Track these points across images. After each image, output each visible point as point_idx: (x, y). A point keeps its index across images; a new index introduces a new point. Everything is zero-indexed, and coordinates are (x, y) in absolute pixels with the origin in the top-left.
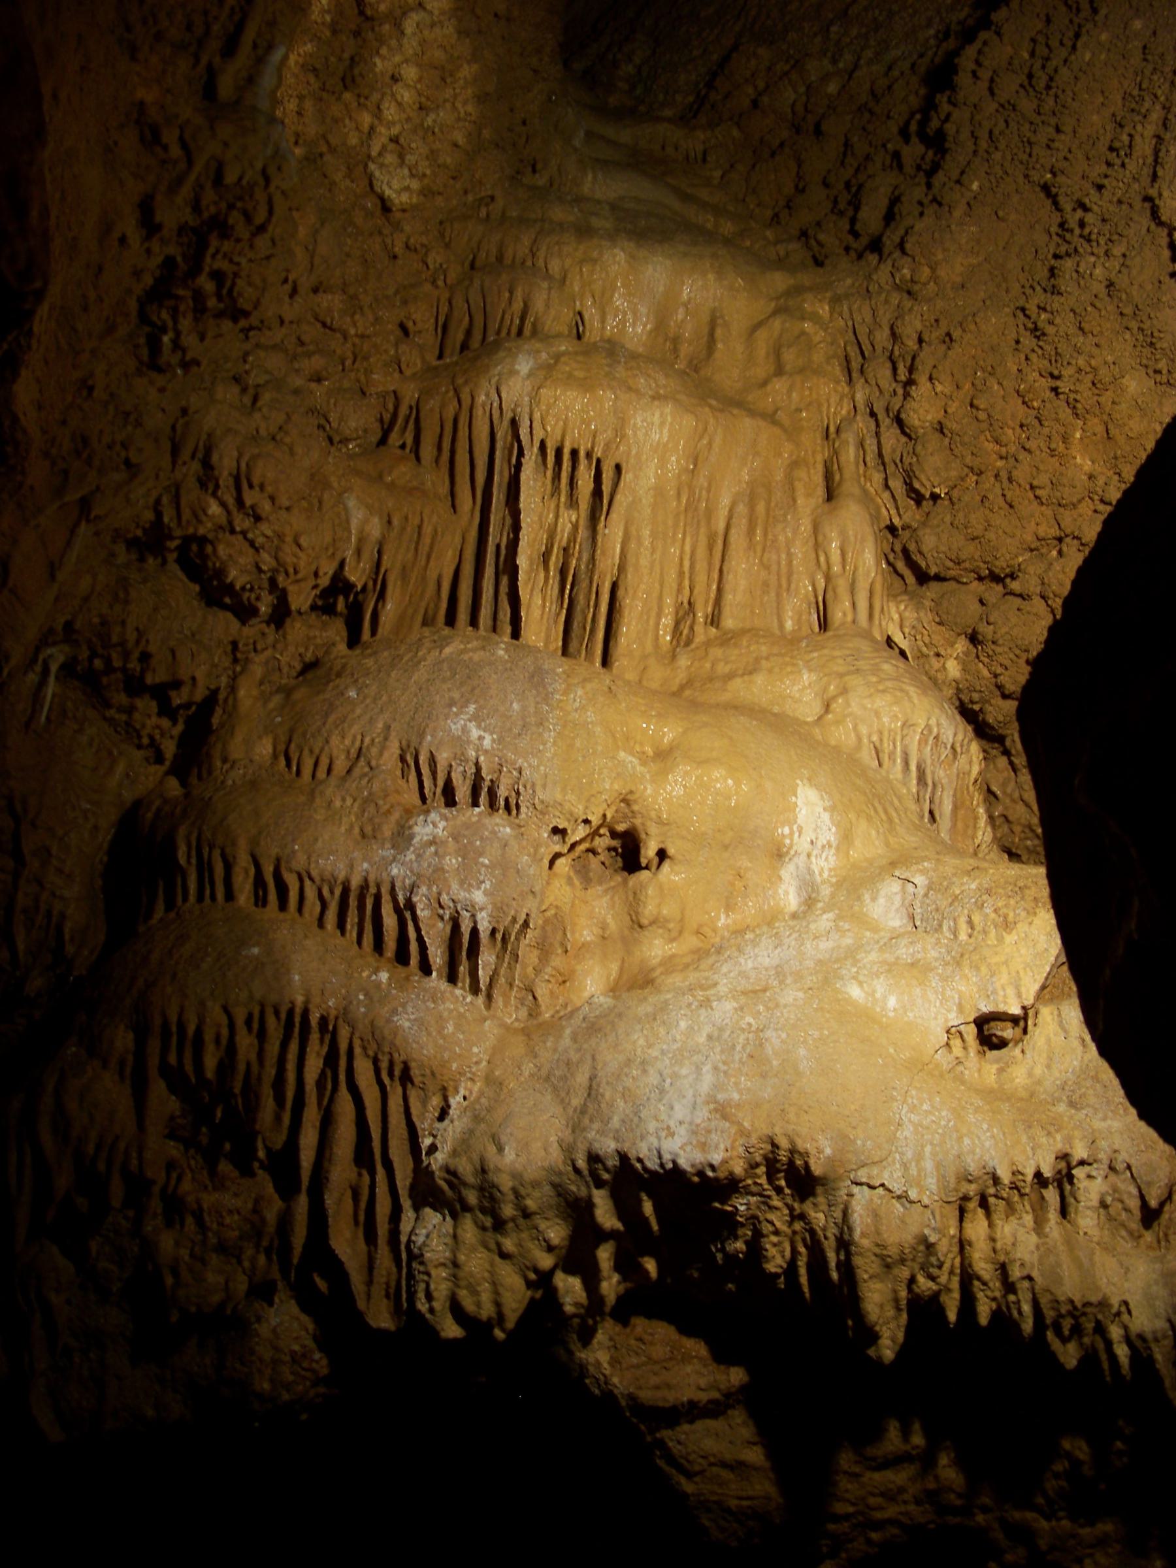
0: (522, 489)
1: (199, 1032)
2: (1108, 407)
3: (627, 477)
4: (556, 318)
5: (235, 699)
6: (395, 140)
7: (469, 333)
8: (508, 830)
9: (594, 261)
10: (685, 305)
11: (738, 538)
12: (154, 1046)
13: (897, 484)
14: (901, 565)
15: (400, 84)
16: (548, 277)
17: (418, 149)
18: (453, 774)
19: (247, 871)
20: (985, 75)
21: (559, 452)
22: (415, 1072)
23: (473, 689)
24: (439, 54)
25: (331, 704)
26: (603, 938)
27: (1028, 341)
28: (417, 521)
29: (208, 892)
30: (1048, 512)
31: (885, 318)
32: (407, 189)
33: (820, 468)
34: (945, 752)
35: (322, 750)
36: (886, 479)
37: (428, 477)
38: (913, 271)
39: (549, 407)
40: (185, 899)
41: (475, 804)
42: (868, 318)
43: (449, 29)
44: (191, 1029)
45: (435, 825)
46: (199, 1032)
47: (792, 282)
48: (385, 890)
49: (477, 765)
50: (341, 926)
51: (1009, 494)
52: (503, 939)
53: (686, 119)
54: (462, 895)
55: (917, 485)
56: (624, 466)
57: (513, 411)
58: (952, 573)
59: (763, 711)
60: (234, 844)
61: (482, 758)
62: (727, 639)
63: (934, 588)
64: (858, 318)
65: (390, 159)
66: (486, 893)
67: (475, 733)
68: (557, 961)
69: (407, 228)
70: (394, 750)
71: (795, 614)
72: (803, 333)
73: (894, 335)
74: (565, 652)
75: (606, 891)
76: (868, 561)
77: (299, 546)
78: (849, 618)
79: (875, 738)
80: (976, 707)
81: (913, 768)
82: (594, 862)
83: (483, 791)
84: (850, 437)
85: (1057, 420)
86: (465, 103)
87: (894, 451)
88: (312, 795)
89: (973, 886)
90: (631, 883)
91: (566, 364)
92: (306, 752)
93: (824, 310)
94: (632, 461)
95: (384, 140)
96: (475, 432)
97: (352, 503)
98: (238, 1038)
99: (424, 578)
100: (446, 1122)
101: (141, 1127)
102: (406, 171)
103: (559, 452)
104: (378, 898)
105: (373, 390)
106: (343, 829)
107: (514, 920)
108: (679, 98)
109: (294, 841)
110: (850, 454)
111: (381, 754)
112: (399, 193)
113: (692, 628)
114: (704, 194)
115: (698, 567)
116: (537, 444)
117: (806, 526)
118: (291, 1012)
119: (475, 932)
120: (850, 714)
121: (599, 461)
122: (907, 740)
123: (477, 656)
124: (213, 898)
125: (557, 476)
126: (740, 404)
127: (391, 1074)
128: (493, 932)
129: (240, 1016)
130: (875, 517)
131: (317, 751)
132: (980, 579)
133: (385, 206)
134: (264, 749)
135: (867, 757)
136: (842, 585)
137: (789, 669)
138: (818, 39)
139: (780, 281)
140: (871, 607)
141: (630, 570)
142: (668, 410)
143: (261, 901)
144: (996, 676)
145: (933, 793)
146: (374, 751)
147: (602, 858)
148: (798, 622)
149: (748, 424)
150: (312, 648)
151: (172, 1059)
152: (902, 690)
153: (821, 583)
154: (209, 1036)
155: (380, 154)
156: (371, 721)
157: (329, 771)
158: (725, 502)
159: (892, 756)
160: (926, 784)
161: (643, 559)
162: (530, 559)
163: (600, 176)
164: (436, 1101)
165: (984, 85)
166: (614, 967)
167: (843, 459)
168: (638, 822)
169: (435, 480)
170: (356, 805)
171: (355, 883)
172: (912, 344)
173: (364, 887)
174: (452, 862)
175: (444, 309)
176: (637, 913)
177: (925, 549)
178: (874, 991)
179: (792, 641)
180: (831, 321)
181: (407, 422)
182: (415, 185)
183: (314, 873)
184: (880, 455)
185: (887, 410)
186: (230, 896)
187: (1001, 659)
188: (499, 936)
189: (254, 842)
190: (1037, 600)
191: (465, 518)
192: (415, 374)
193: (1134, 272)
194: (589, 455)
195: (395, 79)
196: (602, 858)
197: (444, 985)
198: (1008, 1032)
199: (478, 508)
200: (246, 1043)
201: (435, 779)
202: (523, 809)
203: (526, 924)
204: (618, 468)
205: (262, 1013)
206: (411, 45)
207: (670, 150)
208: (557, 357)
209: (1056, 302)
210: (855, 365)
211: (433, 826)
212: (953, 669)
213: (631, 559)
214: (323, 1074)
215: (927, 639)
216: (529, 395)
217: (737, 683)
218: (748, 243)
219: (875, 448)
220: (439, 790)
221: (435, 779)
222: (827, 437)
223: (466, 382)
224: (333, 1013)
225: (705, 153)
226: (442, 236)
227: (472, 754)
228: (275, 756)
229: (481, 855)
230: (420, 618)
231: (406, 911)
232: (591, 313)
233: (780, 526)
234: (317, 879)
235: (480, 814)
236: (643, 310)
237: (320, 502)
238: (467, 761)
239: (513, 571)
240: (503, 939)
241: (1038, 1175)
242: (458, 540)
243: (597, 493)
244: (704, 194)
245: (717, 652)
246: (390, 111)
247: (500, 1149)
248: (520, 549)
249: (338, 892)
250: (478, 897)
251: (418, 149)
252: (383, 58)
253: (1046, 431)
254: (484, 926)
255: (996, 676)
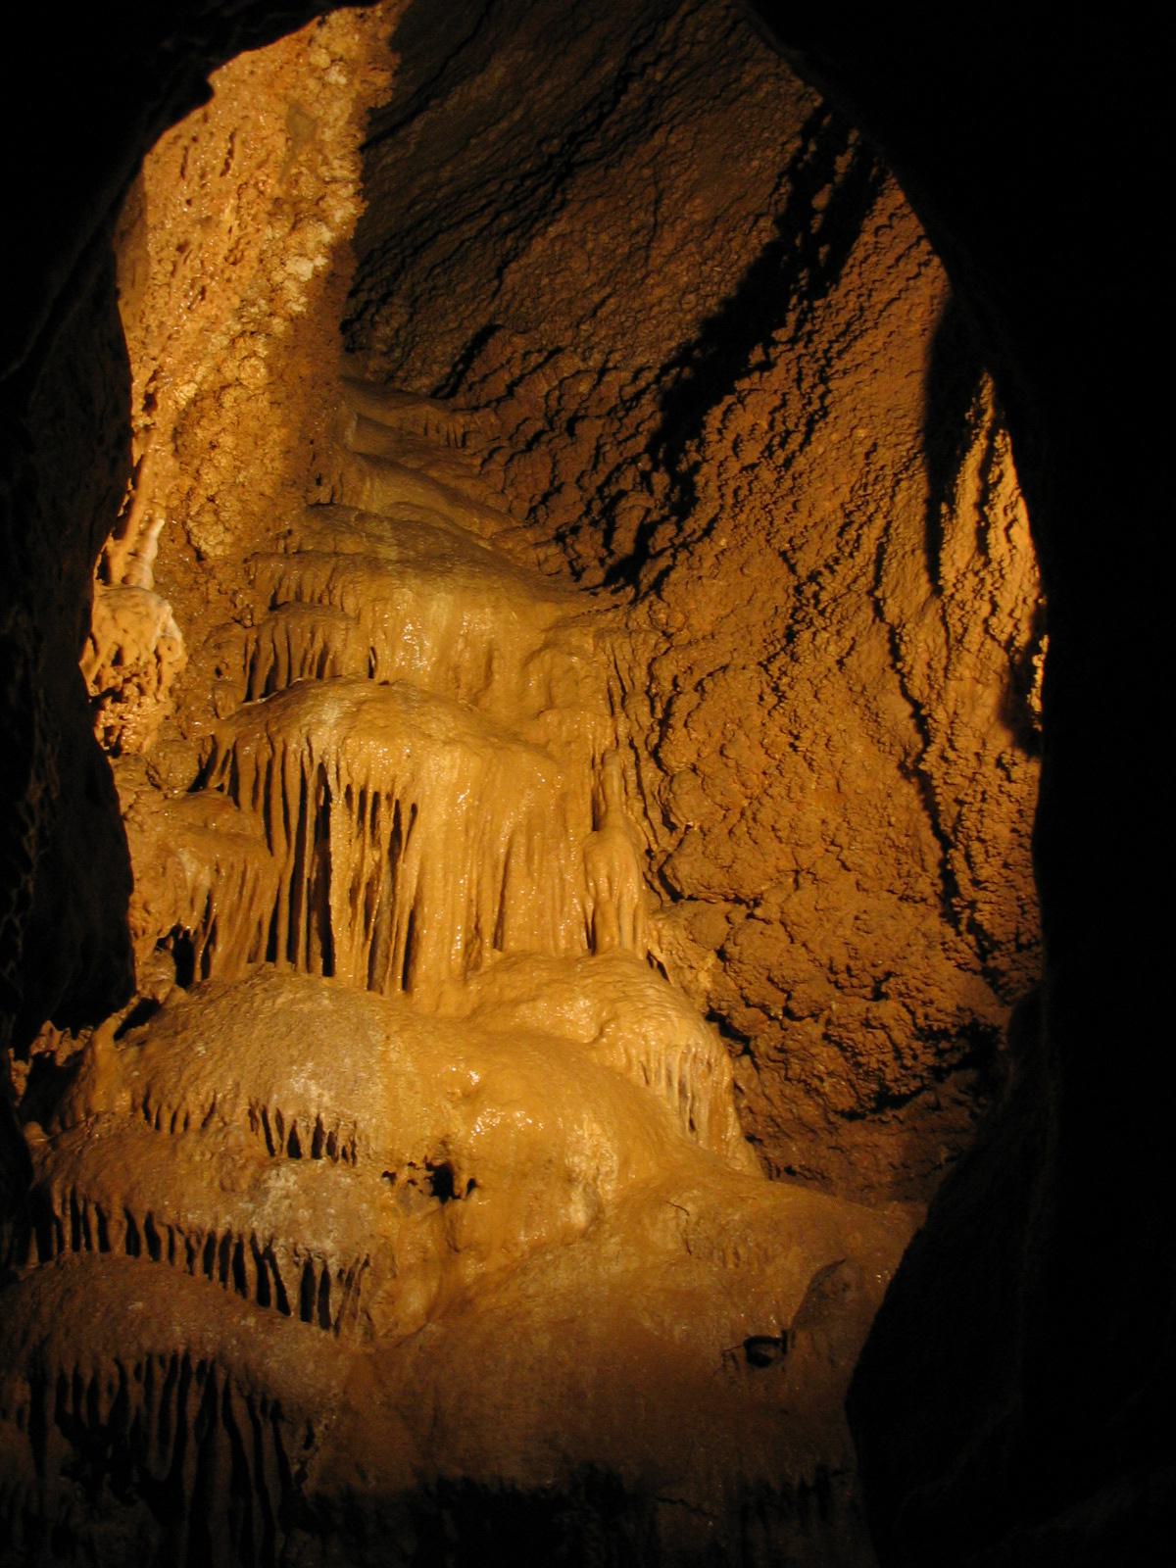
0: (333, 833)
1: (94, 1384)
2: (839, 764)
3: (422, 815)
4: (350, 657)
5: (93, 1052)
6: (211, 499)
7: (275, 669)
8: (349, 1180)
9: (386, 600)
10: (465, 636)
11: (517, 864)
12: (51, 1397)
13: (655, 815)
14: (657, 884)
15: (217, 451)
16: (346, 617)
17: (231, 506)
18: (298, 1129)
19: (121, 1224)
20: (730, 436)
21: (363, 794)
22: (285, 1409)
23: (309, 1046)
24: (253, 425)
25: (183, 1060)
26: (425, 1260)
27: (771, 699)
28: (241, 868)
29: (83, 1241)
30: (788, 849)
31: (645, 657)
32: (222, 543)
33: (589, 798)
34: (702, 1068)
35: (179, 1106)
36: (645, 809)
37: (247, 822)
38: (668, 617)
39: (355, 755)
40: (61, 1248)
41: (316, 1155)
42: (629, 657)
43: (264, 402)
44: (88, 1380)
45: (287, 1180)
46: (94, 1384)
47: (559, 613)
48: (246, 1241)
49: (318, 1119)
50: (207, 1269)
51: (754, 832)
52: (348, 1279)
53: (443, 393)
54: (315, 1244)
55: (673, 820)
56: (419, 807)
57: (322, 757)
58: (703, 895)
59: (548, 1037)
60: (109, 1199)
61: (323, 1115)
62: (513, 963)
63: (688, 909)
64: (620, 657)
65: (208, 518)
66: (335, 1241)
67: (314, 1090)
68: (387, 1285)
69: (220, 576)
70: (243, 1107)
71: (568, 935)
72: (572, 668)
73: (652, 677)
74: (370, 987)
75: (425, 1217)
76: (632, 889)
77: (148, 912)
78: (616, 942)
79: (643, 1058)
80: (724, 1013)
81: (676, 1085)
82: (413, 1191)
83: (323, 1143)
84: (613, 770)
85: (796, 773)
86: (272, 460)
87: (652, 784)
88: (174, 1151)
89: (736, 1217)
90: (447, 1212)
91: (369, 713)
92: (164, 1108)
93: (589, 644)
94: (427, 800)
95: (203, 500)
96: (288, 784)
97: (185, 857)
98: (130, 1387)
99: (247, 919)
100: (312, 1449)
101: (40, 1466)
102: (221, 528)
103: (363, 794)
104: (239, 1248)
105: (195, 735)
106: (204, 1184)
107: (358, 1260)
108: (436, 368)
109: (163, 1197)
110: (615, 785)
111: (233, 1111)
112: (214, 547)
113: (480, 952)
114: (467, 487)
115: (484, 895)
116: (343, 790)
117: (575, 856)
118: (174, 1359)
119: (325, 1274)
120: (622, 1038)
121: (397, 802)
122: (670, 1059)
123: (306, 1007)
124: (89, 1246)
125: (362, 817)
126: (515, 738)
127: (263, 1411)
128: (341, 1272)
129: (130, 1365)
130: (636, 846)
131: (175, 1107)
132: (727, 900)
133: (200, 556)
134: (124, 1100)
135: (636, 1074)
136: (610, 910)
137: (567, 995)
138: (570, 333)
139: (548, 612)
140: (635, 929)
141: (426, 903)
142: (457, 754)
143: (133, 1247)
144: (741, 988)
145: (692, 1105)
146: (227, 1107)
147: (419, 1187)
148: (570, 940)
149: (525, 760)
150: (149, 986)
151: (69, 1408)
152: (665, 1016)
153: (590, 906)
154: (103, 1387)
155: (198, 513)
156: (222, 1078)
157: (186, 1124)
158: (507, 827)
159: (658, 1072)
160: (686, 1097)
161: (435, 892)
162: (341, 898)
163: (377, 483)
164: (302, 1431)
165: (728, 443)
166: (434, 1285)
167: (608, 792)
168: (453, 1158)
169: (251, 824)
170: (215, 1159)
171: (220, 1232)
172: (668, 686)
173: (228, 1236)
174: (304, 1214)
175: (252, 647)
176: (454, 1239)
177: (680, 875)
178: (663, 1322)
179: (568, 962)
180: (594, 655)
181: (224, 764)
182: (229, 538)
183: (184, 1227)
184: (639, 785)
185: (646, 744)
186: (105, 1246)
187: (747, 976)
188: (345, 1276)
189: (127, 1199)
190: (777, 925)
191: (282, 860)
192: (230, 718)
193: (863, 657)
194: (389, 797)
195: (213, 447)
196: (419, 1187)
197: (302, 1325)
198: (772, 1352)
199: (293, 851)
200: (135, 1390)
201: (282, 1138)
202: (359, 1159)
203: (366, 1263)
204: (414, 809)
205: (149, 1363)
206: (228, 417)
207: (432, 433)
208: (360, 703)
209: (796, 670)
210: (617, 699)
211: (285, 1180)
212: (705, 981)
213: (427, 893)
214: (201, 1413)
215: (681, 954)
216: (336, 744)
217: (524, 1010)
218: (510, 545)
219: (634, 778)
220: (285, 1143)
221: (282, 1138)
222: (593, 766)
223: (279, 731)
224: (211, 1358)
225: (464, 435)
226: (247, 573)
227: (313, 1111)
228: (134, 1108)
229: (329, 1205)
230: (245, 957)
231: (265, 1259)
232: (384, 653)
233: (552, 856)
234: (186, 1231)
235: (323, 1166)
236: (428, 644)
237: (164, 868)
238: (309, 1117)
239: (326, 911)
240: (348, 1279)
241: (803, 1484)
242: (276, 881)
243: (396, 834)
244: (467, 487)
245: (503, 978)
246: (209, 476)
247: (364, 1478)
248: (332, 890)
249: (204, 1242)
250: (328, 1245)
251: (231, 506)
252: (204, 429)
253: (786, 781)
254: (333, 1270)
255: (741, 988)
